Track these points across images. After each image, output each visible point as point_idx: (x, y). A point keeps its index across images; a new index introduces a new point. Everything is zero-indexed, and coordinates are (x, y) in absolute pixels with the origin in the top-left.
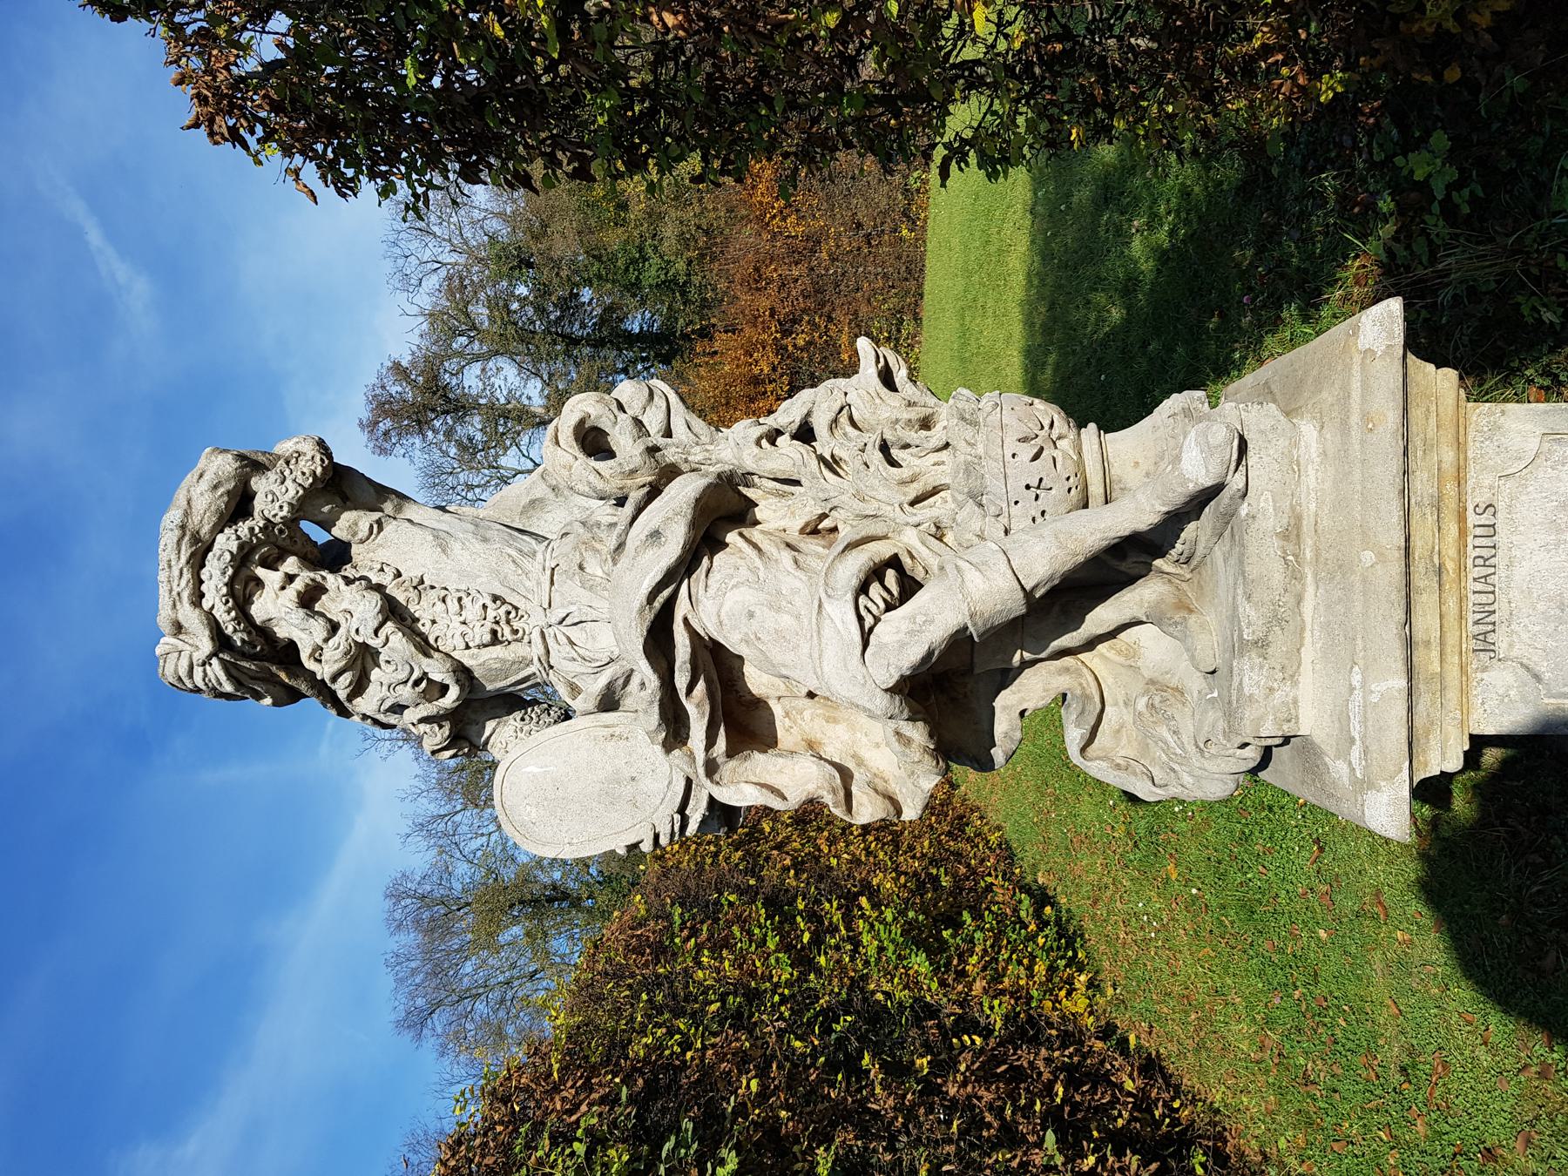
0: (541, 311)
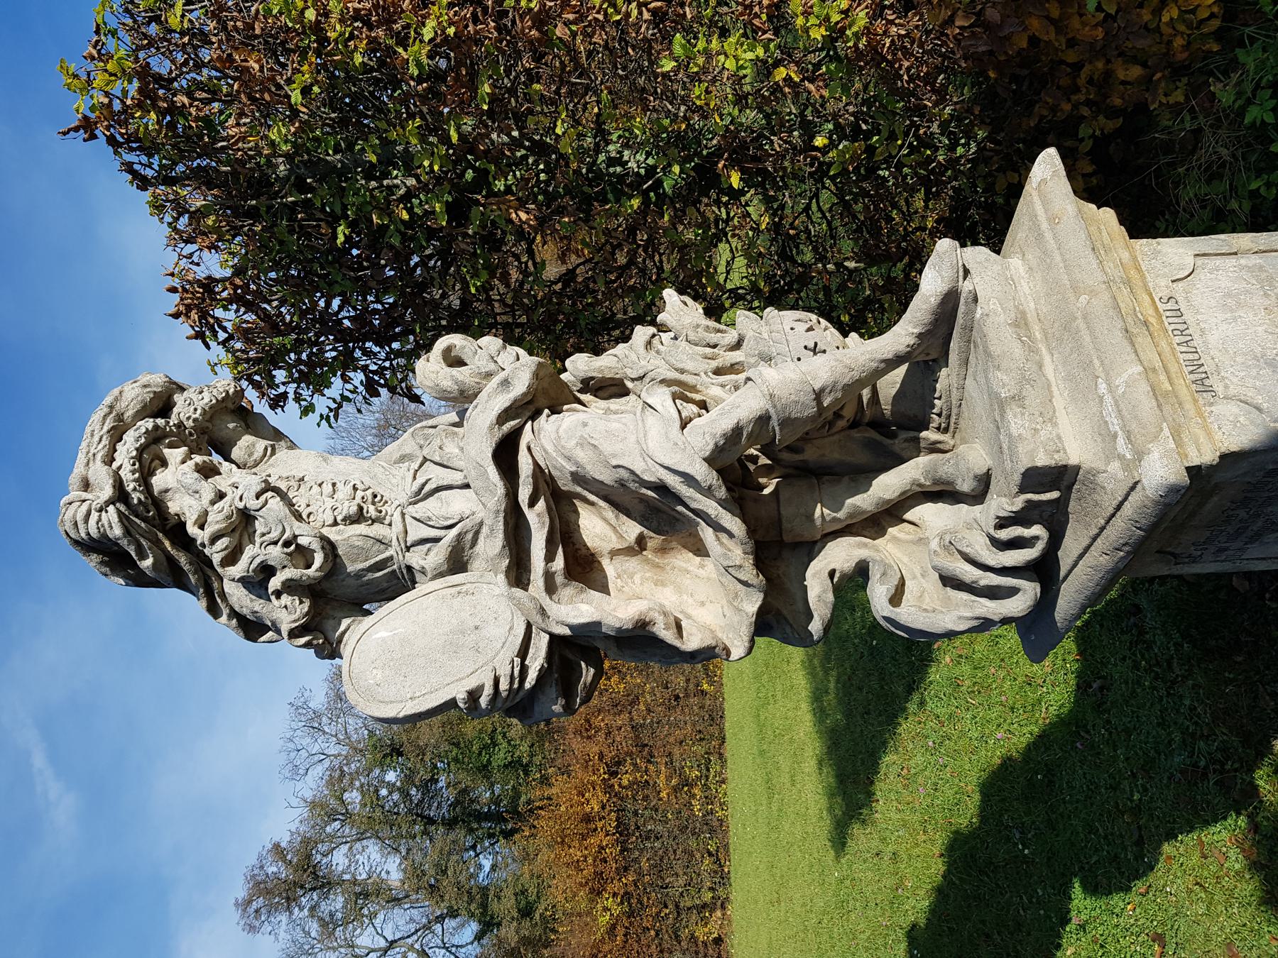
0: (406, 795)
